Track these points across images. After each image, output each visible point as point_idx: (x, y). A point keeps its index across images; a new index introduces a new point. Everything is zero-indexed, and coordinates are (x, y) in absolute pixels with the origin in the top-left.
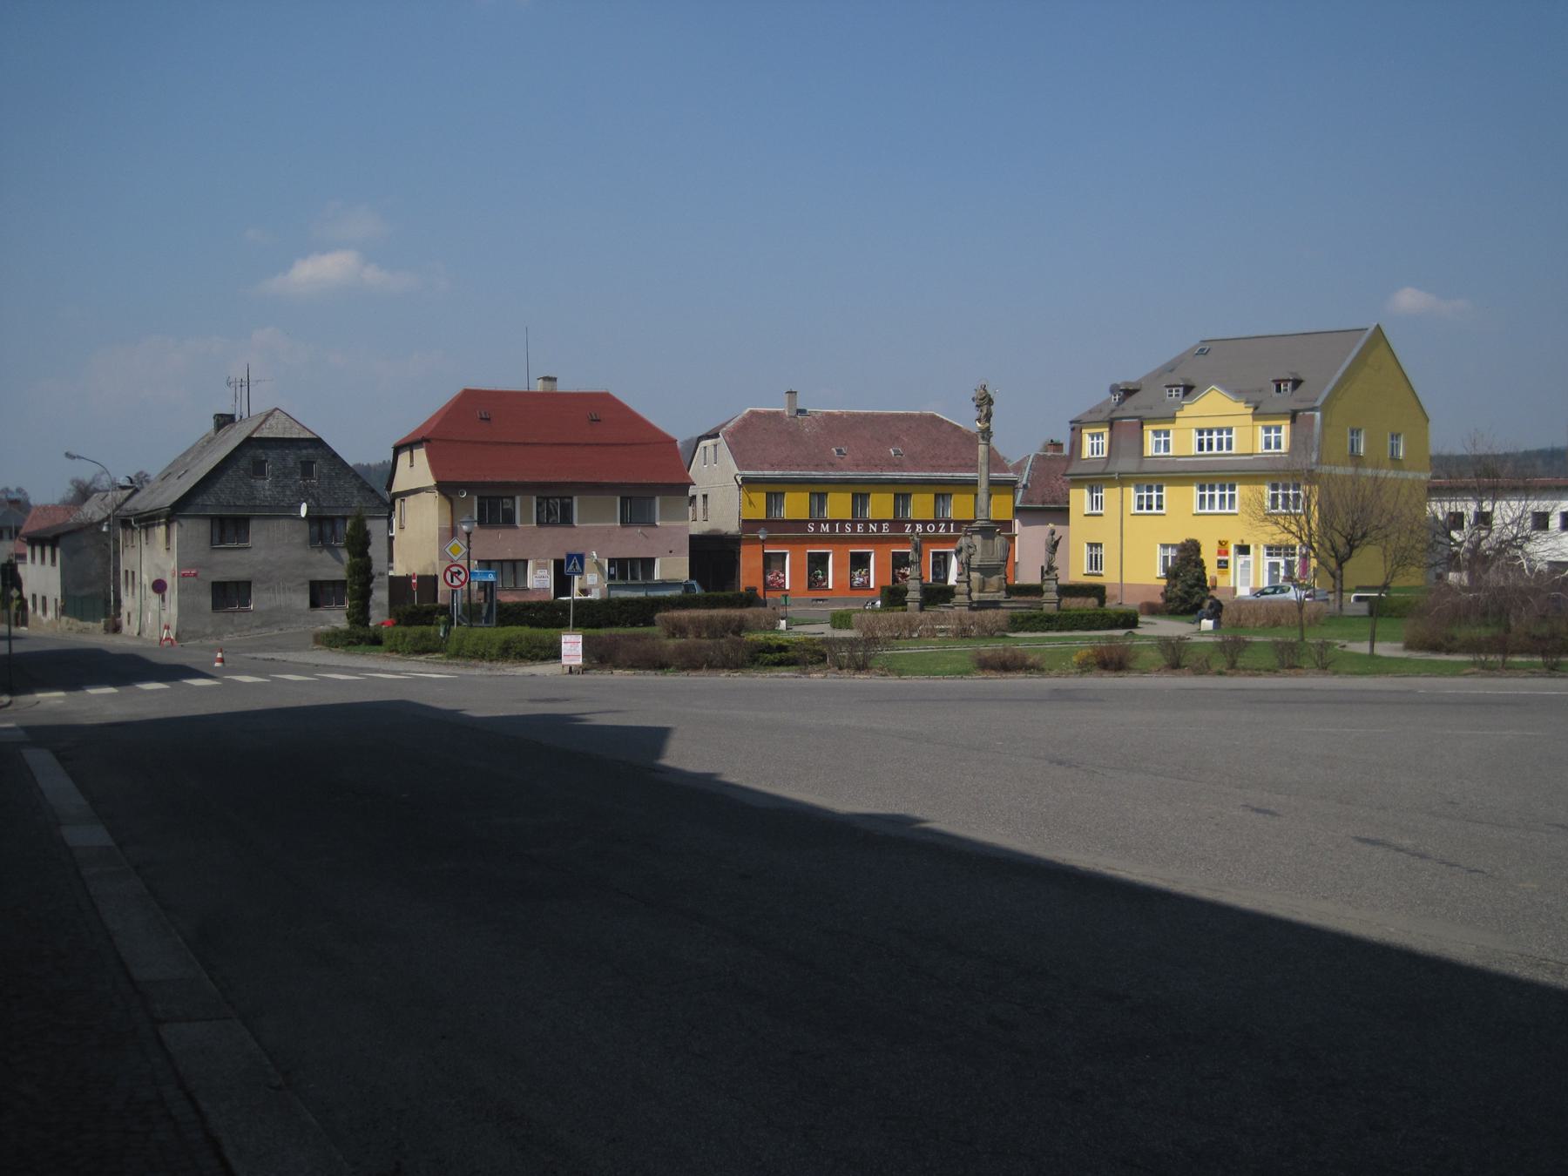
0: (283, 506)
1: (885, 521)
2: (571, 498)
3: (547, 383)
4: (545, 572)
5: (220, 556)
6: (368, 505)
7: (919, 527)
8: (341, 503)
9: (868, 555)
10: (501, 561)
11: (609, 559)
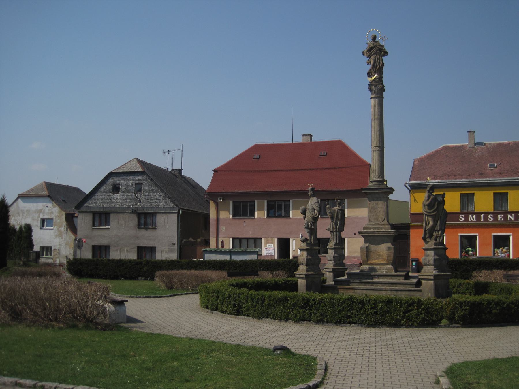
0: (125, 207)
2: (289, 201)
3: (304, 137)
4: (271, 246)
5: (97, 233)
6: (167, 206)
8: (154, 205)
9: (507, 238)
10: (247, 239)
11: (278, 239)
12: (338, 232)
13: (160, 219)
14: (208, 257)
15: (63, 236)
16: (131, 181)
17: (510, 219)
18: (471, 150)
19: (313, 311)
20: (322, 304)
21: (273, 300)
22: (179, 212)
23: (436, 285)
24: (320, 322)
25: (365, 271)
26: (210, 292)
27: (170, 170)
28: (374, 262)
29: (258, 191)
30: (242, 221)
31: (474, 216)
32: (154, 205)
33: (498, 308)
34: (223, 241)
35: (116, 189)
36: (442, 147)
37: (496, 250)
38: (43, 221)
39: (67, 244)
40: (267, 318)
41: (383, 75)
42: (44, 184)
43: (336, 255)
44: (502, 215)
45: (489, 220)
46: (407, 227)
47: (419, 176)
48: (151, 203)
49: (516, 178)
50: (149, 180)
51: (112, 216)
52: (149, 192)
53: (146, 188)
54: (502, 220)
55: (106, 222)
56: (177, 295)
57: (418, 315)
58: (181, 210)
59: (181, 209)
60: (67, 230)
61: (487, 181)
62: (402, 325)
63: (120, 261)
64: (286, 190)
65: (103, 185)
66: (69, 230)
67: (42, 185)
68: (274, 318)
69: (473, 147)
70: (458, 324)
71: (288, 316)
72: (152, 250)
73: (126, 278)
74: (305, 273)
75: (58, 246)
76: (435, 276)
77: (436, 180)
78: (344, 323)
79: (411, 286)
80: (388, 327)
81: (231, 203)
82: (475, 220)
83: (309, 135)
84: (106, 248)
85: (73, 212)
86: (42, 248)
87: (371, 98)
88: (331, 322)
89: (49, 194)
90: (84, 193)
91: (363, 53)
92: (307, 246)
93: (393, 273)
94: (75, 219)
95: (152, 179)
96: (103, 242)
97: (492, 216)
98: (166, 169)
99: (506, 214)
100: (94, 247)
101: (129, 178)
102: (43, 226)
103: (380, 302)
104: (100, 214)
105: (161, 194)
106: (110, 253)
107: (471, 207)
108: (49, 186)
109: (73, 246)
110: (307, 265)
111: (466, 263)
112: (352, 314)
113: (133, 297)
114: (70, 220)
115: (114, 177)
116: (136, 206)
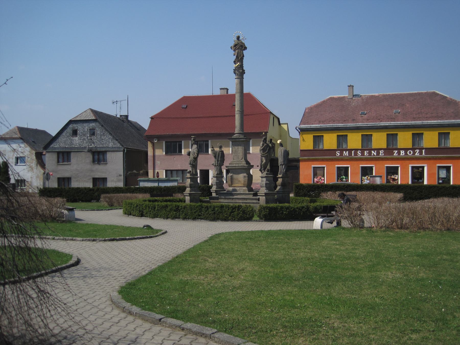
0: (83, 147)
1: (381, 149)
3: (222, 90)
5: (61, 168)
6: (115, 146)
7: (402, 153)
9: (371, 168)
10: (177, 170)
12: (219, 167)
13: (109, 156)
14: (142, 184)
15: (34, 171)
16: (87, 127)
17: (373, 154)
18: (350, 101)
19: (181, 213)
20: (186, 209)
21: (160, 207)
22: (124, 150)
23: (266, 198)
24: (185, 218)
25: (230, 191)
26: (127, 204)
27: (118, 116)
28: (236, 185)
29: (184, 133)
30: (172, 157)
31: (347, 152)
32: (105, 146)
33: (288, 210)
34: (158, 173)
35: (75, 133)
36: (328, 98)
37: (363, 177)
38: (17, 159)
39: (37, 177)
40: (157, 217)
41: (244, 63)
42: (16, 128)
43: (217, 181)
44: (368, 151)
45: (358, 155)
46: (298, 161)
47: (307, 121)
48: (102, 144)
49: (378, 123)
50: (101, 126)
51: (72, 154)
52: (101, 135)
53: (99, 132)
54: (368, 155)
55: (68, 159)
56: (113, 209)
57: (238, 214)
58: (125, 149)
59: (126, 148)
60: (37, 166)
61: (356, 126)
62: (229, 220)
63: (78, 189)
64: (205, 132)
65: (65, 130)
66: (38, 165)
67: (15, 129)
68: (160, 217)
69: (352, 99)
70: (263, 219)
71: (168, 216)
72: (104, 180)
73: (83, 201)
74: (189, 192)
75: (30, 179)
76: (265, 193)
77: (319, 124)
78: (197, 219)
79: (256, 200)
80: (221, 221)
81: (164, 142)
82: (347, 155)
83: (225, 89)
84: (69, 179)
85: (41, 151)
86: (17, 181)
87: (235, 78)
88: (190, 219)
89: (21, 136)
90: (50, 135)
91: (231, 48)
92: (190, 176)
93: (247, 192)
94: (43, 156)
95: (102, 125)
96: (67, 175)
97: (360, 152)
98: (115, 116)
99: (370, 150)
100: (59, 179)
101: (85, 125)
102: (17, 163)
103: (217, 207)
104: (63, 153)
105: (110, 137)
106: (72, 184)
107: (345, 145)
108: (21, 130)
109: (42, 179)
110: (190, 187)
111: (323, 187)
112: (201, 214)
113: (83, 210)
114: (39, 157)
115: (73, 124)
116: (91, 147)
